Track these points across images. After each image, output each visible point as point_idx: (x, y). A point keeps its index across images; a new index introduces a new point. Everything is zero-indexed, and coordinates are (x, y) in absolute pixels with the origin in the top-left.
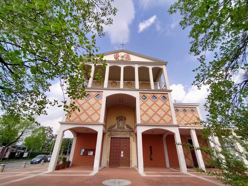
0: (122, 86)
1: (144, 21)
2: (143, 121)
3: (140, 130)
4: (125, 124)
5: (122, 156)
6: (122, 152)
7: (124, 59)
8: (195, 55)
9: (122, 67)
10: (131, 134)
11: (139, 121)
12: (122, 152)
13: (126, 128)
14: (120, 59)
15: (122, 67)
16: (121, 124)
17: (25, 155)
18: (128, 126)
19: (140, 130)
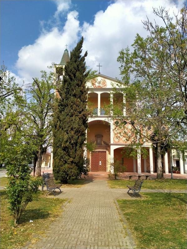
0: (99, 114)
1: (41, 32)
2: (116, 142)
3: (113, 148)
4: (102, 140)
5: (100, 164)
6: (100, 162)
7: (101, 85)
8: (75, 18)
9: (99, 93)
10: (107, 149)
11: (112, 142)
12: (100, 162)
13: (103, 144)
14: (97, 85)
15: (99, 93)
16: (99, 141)
17: (3, 165)
18: (104, 142)
19: (113, 148)
